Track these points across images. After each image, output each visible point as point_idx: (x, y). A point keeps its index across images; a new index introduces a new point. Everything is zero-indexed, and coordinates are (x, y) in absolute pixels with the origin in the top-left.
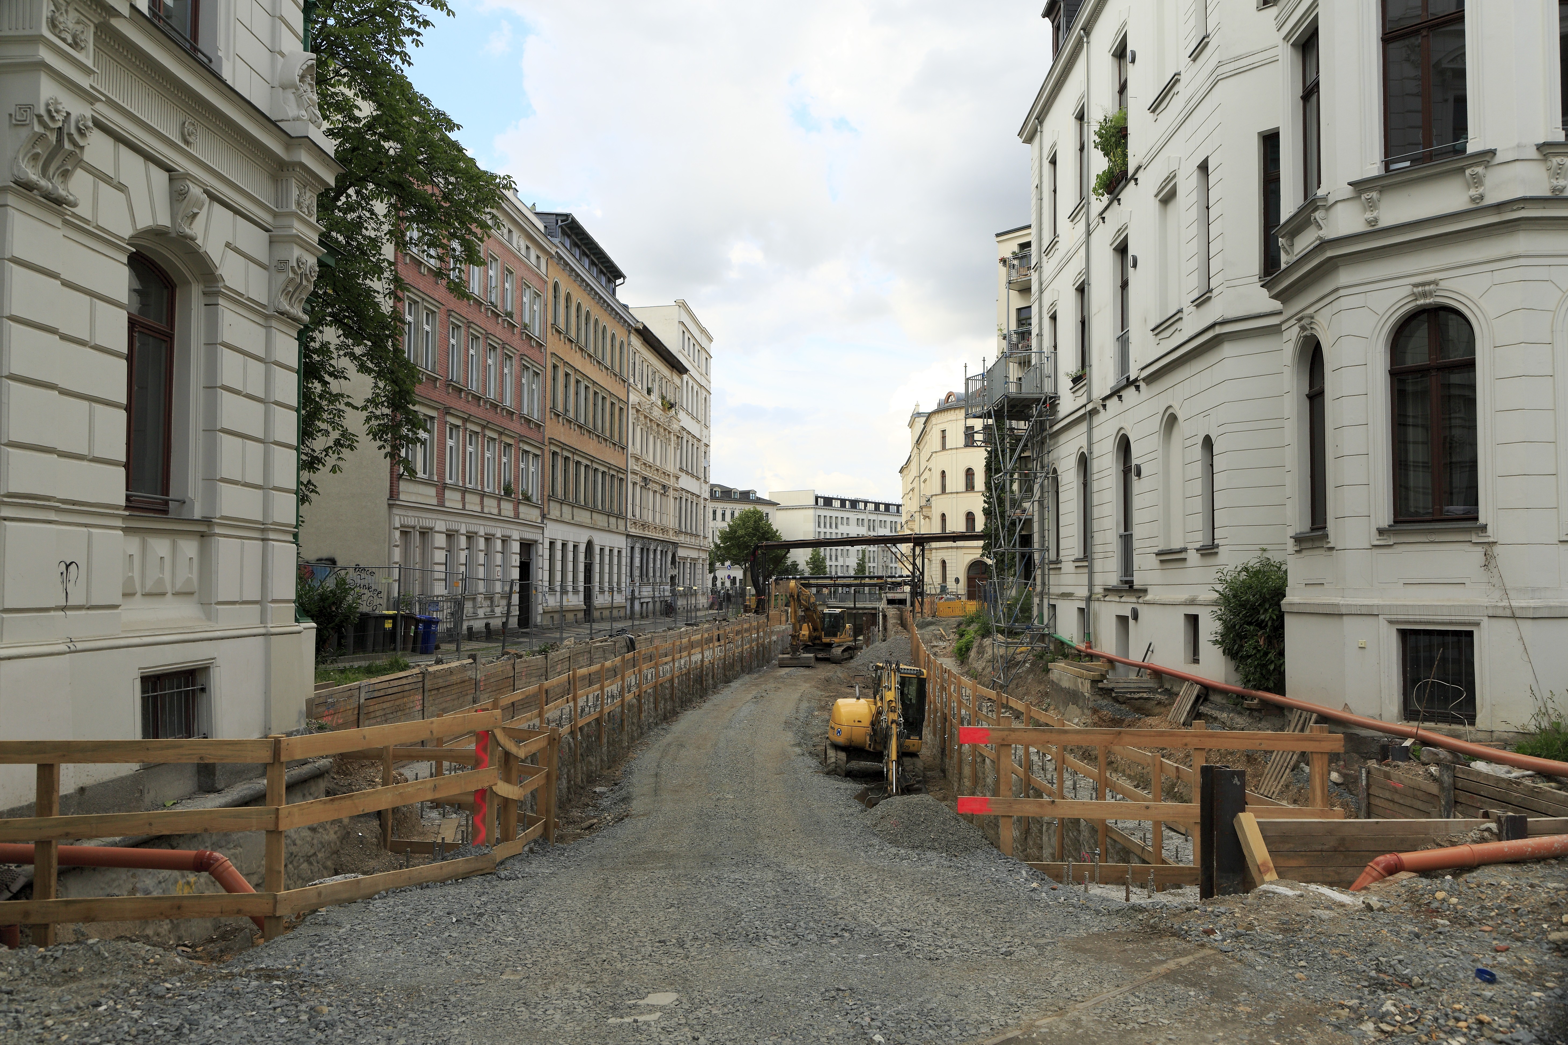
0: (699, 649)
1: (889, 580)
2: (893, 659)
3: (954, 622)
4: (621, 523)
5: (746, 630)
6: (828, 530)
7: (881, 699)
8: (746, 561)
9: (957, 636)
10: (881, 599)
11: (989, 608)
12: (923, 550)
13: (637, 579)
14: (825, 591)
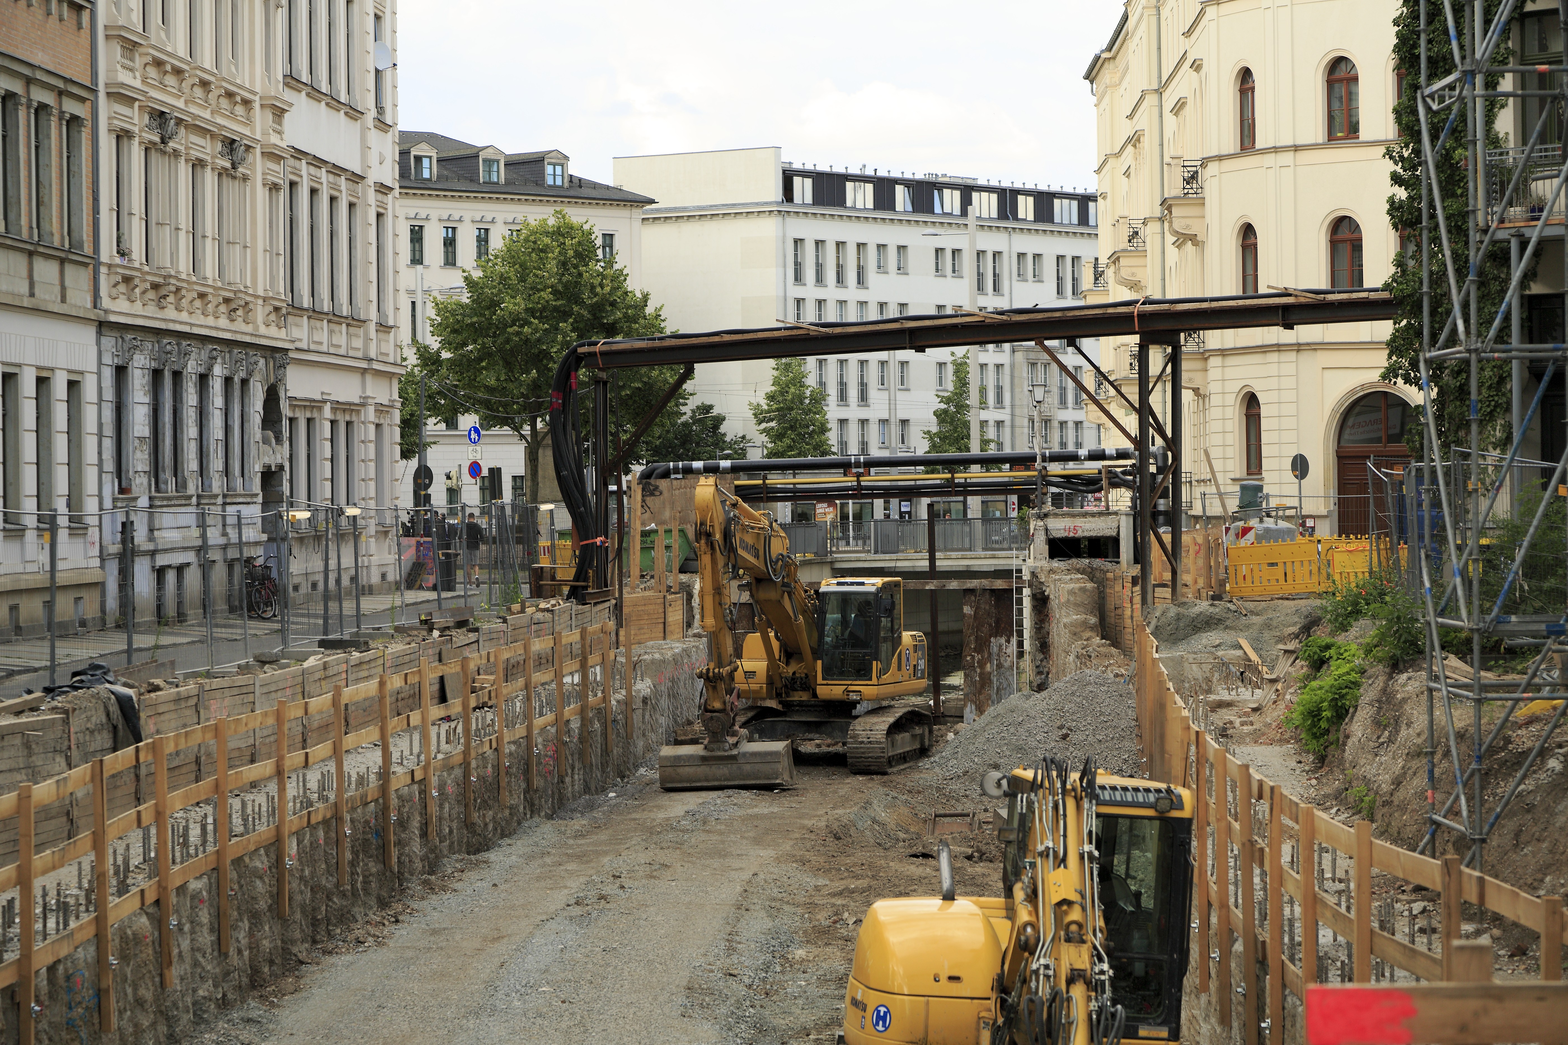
0: (372, 733)
1: (1055, 468)
2: (1073, 755)
3: (1289, 616)
4: (78, 279)
5: (543, 661)
6: (831, 292)
7: (1033, 896)
8: (533, 411)
9: (1301, 668)
10: (1025, 539)
11: (1414, 560)
12: (1174, 359)
13: (140, 484)
14: (825, 513)
